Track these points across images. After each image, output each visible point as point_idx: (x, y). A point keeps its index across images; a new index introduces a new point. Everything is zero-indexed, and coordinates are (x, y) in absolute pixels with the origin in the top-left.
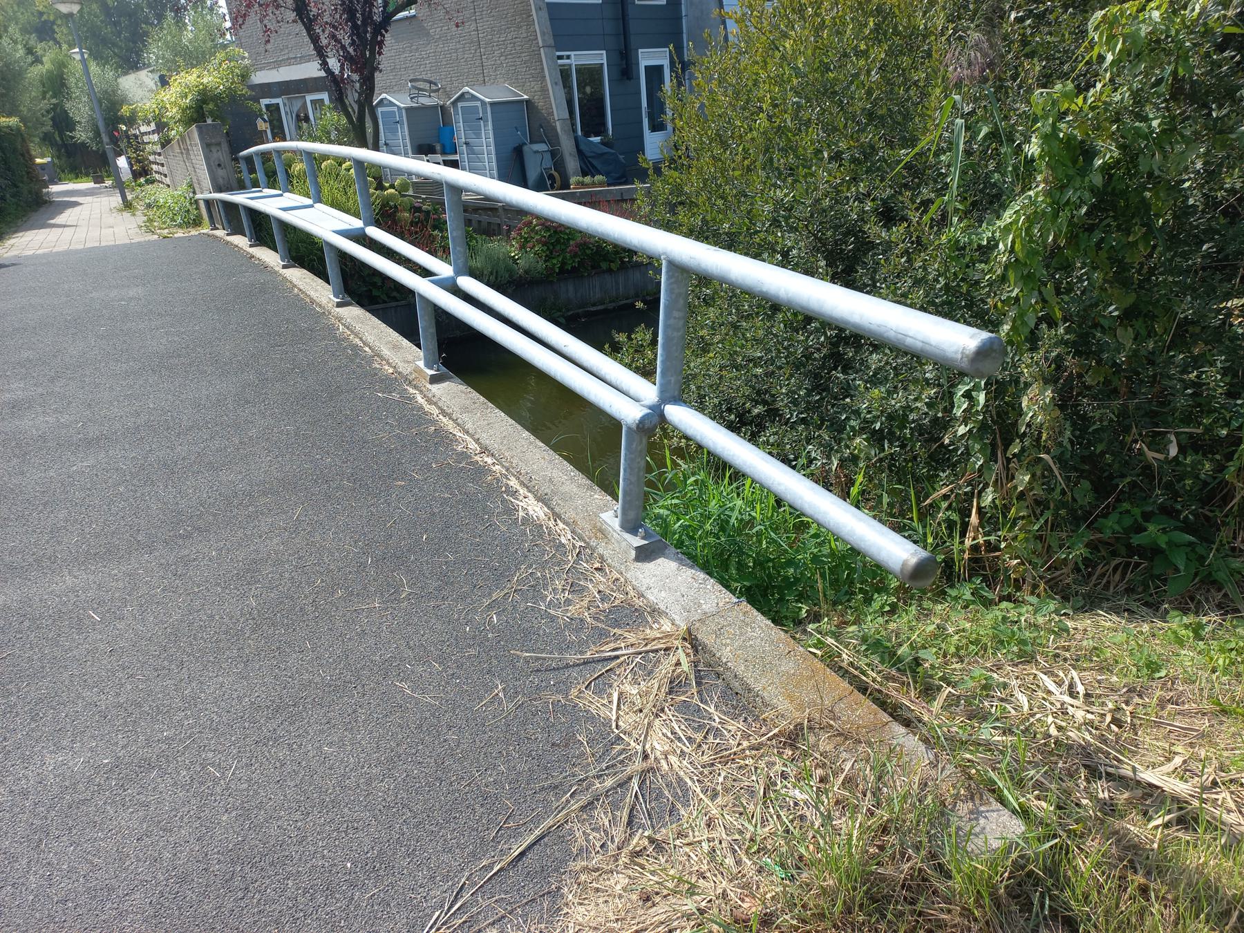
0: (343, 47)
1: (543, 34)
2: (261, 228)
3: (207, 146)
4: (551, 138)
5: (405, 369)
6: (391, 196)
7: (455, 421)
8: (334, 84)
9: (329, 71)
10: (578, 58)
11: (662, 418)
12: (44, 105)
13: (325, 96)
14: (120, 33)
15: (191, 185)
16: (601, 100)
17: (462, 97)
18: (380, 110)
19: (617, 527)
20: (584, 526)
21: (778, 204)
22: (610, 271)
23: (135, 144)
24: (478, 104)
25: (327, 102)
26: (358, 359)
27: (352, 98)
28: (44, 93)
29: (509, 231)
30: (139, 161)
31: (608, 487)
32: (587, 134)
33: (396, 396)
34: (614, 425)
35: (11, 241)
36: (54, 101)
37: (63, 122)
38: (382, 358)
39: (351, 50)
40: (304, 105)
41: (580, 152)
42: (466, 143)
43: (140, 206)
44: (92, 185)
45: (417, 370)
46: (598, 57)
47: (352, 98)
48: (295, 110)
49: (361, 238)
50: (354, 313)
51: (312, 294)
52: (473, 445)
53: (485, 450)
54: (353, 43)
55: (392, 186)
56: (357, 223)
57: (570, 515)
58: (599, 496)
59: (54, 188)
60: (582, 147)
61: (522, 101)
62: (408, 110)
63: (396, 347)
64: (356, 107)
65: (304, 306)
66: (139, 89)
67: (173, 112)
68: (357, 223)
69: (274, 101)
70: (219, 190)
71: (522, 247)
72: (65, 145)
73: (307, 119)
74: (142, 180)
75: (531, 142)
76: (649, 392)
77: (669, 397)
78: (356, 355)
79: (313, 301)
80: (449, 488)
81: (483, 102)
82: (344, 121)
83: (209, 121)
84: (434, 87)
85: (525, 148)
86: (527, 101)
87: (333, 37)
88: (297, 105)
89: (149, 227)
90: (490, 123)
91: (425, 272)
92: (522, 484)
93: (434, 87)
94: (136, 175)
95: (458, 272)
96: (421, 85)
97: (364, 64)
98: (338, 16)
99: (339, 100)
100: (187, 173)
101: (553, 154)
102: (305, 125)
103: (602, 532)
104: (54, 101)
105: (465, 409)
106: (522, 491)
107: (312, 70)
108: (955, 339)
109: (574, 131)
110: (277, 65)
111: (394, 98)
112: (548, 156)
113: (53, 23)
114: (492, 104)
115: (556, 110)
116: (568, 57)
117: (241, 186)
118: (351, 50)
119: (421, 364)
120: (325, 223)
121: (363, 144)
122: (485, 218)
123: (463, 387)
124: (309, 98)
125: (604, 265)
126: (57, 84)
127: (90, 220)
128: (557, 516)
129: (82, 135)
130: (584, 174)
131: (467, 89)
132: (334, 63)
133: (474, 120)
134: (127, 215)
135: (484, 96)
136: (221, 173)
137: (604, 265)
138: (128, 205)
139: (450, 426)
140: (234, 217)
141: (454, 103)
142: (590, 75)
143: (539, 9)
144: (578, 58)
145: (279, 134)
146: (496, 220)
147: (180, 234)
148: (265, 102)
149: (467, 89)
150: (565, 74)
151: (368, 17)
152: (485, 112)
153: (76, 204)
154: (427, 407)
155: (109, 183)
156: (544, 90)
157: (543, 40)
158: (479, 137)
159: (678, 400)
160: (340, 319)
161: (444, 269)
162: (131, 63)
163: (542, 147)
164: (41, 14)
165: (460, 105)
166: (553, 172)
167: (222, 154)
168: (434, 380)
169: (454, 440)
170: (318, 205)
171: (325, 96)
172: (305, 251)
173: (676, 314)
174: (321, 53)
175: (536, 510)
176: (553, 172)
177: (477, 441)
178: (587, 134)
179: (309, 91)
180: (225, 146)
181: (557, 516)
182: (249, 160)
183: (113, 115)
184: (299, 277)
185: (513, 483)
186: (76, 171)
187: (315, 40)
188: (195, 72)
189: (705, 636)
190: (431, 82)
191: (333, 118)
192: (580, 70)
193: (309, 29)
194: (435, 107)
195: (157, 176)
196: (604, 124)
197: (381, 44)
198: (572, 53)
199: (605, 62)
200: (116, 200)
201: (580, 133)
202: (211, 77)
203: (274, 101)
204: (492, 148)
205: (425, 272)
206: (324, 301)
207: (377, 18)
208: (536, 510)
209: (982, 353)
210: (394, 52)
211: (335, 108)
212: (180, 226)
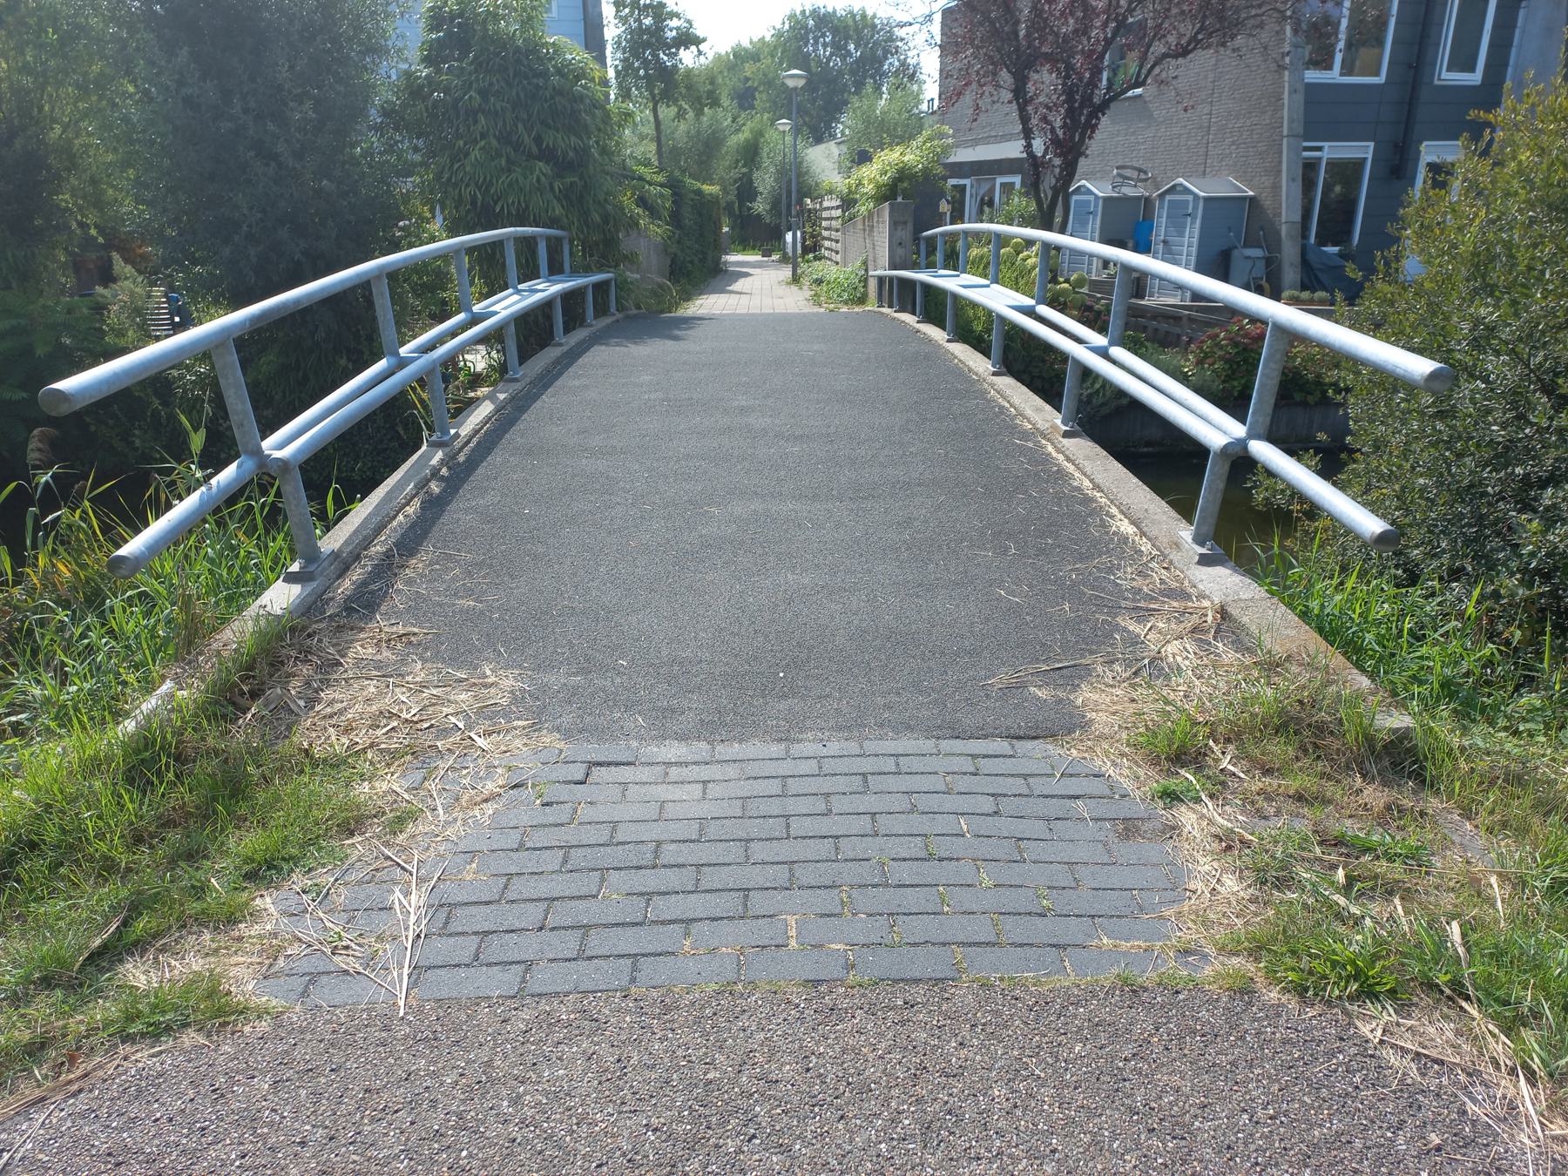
0: (1053, 130)
1: (1291, 121)
2: (934, 305)
3: (894, 224)
4: (1271, 243)
5: (1042, 425)
6: (1065, 290)
7: (1077, 466)
8: (1032, 168)
9: (1031, 155)
10: (1332, 151)
11: (1245, 448)
12: (734, 174)
13: (1017, 180)
14: (815, 100)
15: (865, 263)
16: (1354, 203)
17: (1172, 190)
18: (1075, 198)
19: (1190, 540)
20: (1164, 541)
21: (1477, 321)
22: (1305, 404)
23: (813, 218)
24: (1190, 198)
25: (1018, 186)
26: (1005, 422)
27: (1048, 182)
28: (737, 161)
29: (1189, 343)
30: (813, 236)
31: (1185, 509)
32: (1323, 240)
33: (1030, 444)
34: (1199, 451)
35: (698, 302)
36: (745, 170)
37: (747, 191)
38: (1024, 417)
39: (1060, 133)
40: (992, 189)
41: (1305, 263)
42: (1165, 242)
43: (806, 281)
44: (759, 258)
45: (1054, 427)
46: (1365, 150)
47: (1048, 182)
48: (982, 192)
49: (1030, 312)
50: (1007, 383)
51: (971, 363)
52: (1087, 483)
53: (1097, 487)
54: (1064, 126)
55: (1067, 281)
56: (1030, 302)
57: (1153, 532)
58: (1183, 524)
59: (732, 258)
60: (1311, 257)
61: (1244, 198)
62: (1106, 199)
63: (1038, 410)
64: (1050, 193)
65: (962, 374)
66: (824, 161)
67: (869, 188)
68: (1030, 302)
69: (962, 182)
70: (893, 267)
71: (1200, 362)
72: (741, 216)
73: (991, 203)
74: (811, 256)
75: (1245, 246)
76: (1238, 430)
77: (1252, 435)
78: (1002, 413)
79: (970, 370)
80: (1059, 505)
81: (1196, 196)
82: (1033, 207)
83: (900, 199)
84: (1143, 176)
85: (1235, 253)
86: (1252, 199)
87: (1044, 119)
88: (985, 187)
89: (816, 300)
90: (1198, 221)
91: (1079, 341)
92: (1122, 512)
93: (1143, 176)
94: (806, 250)
95: (1111, 344)
96: (1128, 172)
97: (1070, 150)
98: (1054, 97)
99: (1032, 187)
100: (868, 250)
101: (1269, 261)
102: (987, 209)
103: (1177, 545)
104: (745, 170)
105: (1087, 458)
106: (1119, 516)
107: (1013, 150)
108: (1419, 366)
109: (1305, 236)
110: (975, 143)
111: (1094, 186)
112: (1261, 264)
113: (756, 89)
114: (1206, 199)
115: (1287, 210)
116: (1319, 149)
117: (914, 266)
118: (1060, 133)
119: (1059, 422)
120: (1001, 300)
121: (1048, 226)
122: (1164, 326)
123: (1091, 444)
124: (1000, 180)
125: (1298, 397)
126: (751, 153)
127: (760, 290)
128: (1143, 534)
129: (760, 206)
130: (1304, 288)
131: (1181, 180)
132: (1038, 146)
133: (1179, 216)
134: (794, 288)
135: (1199, 189)
136: (900, 251)
137: (1298, 397)
138: (796, 279)
139: (1071, 468)
140: (904, 295)
141: (1162, 196)
142: (1347, 172)
143: (1293, 91)
144: (1332, 151)
145: (958, 217)
146: (1178, 330)
147: (845, 309)
148: (952, 182)
149: (1181, 180)
150: (1310, 167)
151: (1086, 100)
152: (1195, 208)
153: (747, 275)
154: (1054, 454)
155: (775, 257)
156: (1276, 187)
157: (1290, 128)
158: (1182, 235)
159: (1259, 437)
160: (992, 385)
161: (1099, 340)
162: (819, 135)
163: (1257, 253)
164: (747, 79)
165: (1168, 198)
166: (1263, 282)
167: (905, 234)
168: (1066, 435)
169: (1072, 477)
170: (995, 286)
171: (1017, 180)
172: (970, 326)
173: (1272, 365)
174: (1027, 134)
175: (1127, 528)
176: (1263, 282)
177: (1091, 481)
178: (1323, 240)
179: (1001, 173)
180: (910, 227)
181: (1143, 534)
182: (931, 242)
183: (797, 190)
184: (963, 352)
185: (1114, 510)
186: (745, 244)
187: (1025, 119)
188: (899, 149)
189: (1234, 611)
190: (1140, 171)
191: (1019, 202)
192: (1332, 164)
193: (1022, 110)
194: (1139, 198)
195: (827, 253)
196: (1349, 232)
197: (1094, 128)
198: (1326, 144)
199: (1370, 156)
200: (786, 272)
201: (1312, 240)
202: (910, 156)
203: (962, 182)
204: (1194, 250)
205: (1079, 341)
206: (981, 370)
207: (1096, 100)
208: (1127, 528)
209: (1434, 376)
210: (1108, 134)
211: (1027, 194)
212: (846, 303)
